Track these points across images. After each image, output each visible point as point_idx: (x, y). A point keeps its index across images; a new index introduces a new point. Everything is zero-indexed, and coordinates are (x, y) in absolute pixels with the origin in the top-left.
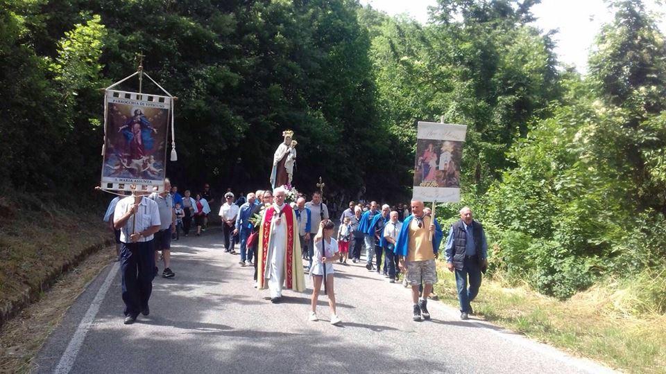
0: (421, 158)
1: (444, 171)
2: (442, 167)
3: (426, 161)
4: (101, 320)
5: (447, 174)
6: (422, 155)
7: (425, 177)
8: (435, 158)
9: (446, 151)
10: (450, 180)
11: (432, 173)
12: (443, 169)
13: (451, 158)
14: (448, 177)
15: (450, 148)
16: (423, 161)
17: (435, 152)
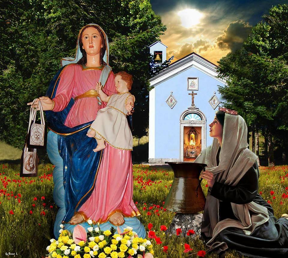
0: (43, 104)
1: (188, 170)
2: (165, 144)
3: (71, 120)
4: (116, 193)
5: (206, 182)
6: (49, 89)
7: (75, 203)
8: (123, 102)
9: (187, 56)
10: (226, 213)
11: (113, 178)
12: (178, 157)
13: (226, 94)
14: (213, 203)
15: (213, 42)
16: (54, 121)
17: (116, 70)
